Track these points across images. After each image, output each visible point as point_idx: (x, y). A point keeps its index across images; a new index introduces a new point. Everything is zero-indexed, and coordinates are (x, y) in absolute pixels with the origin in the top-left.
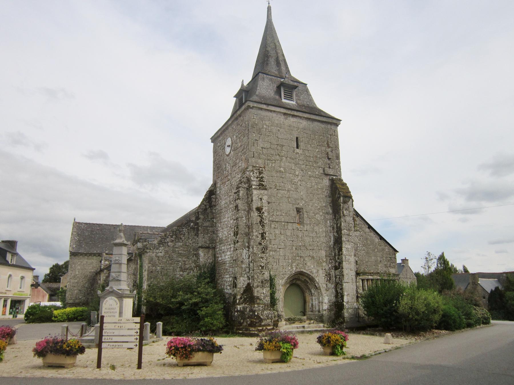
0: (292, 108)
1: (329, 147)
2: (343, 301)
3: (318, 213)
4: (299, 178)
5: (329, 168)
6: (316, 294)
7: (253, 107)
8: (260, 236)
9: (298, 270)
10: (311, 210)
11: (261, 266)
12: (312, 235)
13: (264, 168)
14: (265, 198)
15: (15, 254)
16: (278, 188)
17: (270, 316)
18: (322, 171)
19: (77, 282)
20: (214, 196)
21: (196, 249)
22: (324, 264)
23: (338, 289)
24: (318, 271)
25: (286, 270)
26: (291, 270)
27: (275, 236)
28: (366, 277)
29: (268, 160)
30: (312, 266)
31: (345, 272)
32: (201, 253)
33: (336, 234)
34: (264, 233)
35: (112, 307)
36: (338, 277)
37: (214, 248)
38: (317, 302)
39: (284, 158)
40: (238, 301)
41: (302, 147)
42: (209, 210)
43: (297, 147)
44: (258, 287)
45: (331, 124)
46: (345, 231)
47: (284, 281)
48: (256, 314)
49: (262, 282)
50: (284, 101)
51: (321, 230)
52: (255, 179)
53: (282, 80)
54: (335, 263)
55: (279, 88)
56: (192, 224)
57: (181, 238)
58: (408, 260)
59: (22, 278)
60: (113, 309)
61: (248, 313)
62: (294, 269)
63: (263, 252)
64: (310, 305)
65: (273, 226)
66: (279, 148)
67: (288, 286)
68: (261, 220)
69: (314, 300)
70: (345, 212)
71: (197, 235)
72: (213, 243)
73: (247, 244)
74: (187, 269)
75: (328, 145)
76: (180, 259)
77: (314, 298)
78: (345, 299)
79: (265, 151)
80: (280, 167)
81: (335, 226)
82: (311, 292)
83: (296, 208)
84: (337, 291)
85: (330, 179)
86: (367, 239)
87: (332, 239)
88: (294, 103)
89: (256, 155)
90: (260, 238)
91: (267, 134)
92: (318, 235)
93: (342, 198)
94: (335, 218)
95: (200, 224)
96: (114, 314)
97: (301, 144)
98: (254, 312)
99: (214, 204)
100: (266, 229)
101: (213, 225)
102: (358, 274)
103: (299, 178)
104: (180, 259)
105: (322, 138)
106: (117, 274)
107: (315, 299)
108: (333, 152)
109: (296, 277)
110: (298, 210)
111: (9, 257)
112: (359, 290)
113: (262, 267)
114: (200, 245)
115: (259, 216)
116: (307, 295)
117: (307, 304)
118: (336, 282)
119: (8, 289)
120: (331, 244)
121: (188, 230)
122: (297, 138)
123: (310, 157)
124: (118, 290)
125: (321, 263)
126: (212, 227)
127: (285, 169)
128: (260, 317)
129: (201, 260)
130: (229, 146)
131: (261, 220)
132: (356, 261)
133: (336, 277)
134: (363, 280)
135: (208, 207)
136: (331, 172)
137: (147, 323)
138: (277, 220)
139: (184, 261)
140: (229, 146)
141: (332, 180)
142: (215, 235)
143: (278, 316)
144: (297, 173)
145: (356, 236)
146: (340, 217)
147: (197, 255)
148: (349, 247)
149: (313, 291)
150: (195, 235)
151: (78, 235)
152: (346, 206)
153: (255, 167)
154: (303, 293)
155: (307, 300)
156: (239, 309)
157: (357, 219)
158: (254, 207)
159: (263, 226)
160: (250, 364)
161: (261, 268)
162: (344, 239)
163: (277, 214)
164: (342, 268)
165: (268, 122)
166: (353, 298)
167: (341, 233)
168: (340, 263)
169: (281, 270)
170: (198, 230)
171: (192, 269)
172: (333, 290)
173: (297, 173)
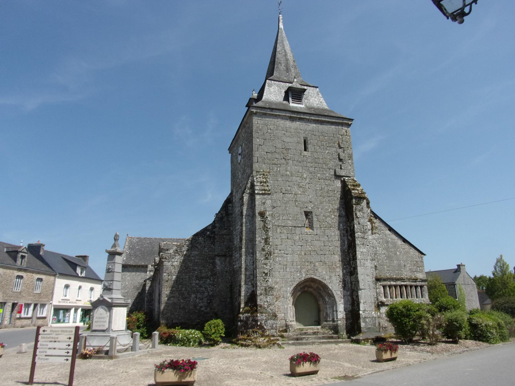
0: (299, 111)
1: (340, 147)
2: (359, 310)
3: (329, 216)
4: (308, 181)
5: (341, 168)
6: (330, 301)
7: (256, 113)
8: (263, 241)
9: (309, 276)
10: (321, 213)
11: (264, 273)
12: (323, 239)
13: (269, 172)
14: (269, 202)
15: (84, 268)
16: (283, 192)
17: (274, 326)
18: (333, 173)
19: (127, 292)
20: (230, 205)
21: (213, 259)
22: (338, 270)
23: (354, 297)
24: (331, 277)
25: (295, 277)
26: (300, 277)
27: (281, 242)
28: (388, 283)
29: (273, 164)
30: (324, 272)
31: (361, 277)
32: (218, 261)
33: (349, 237)
34: (267, 238)
35: (101, 316)
36: (354, 283)
37: (231, 256)
38: (331, 311)
39: (290, 162)
40: (241, 310)
41: (310, 150)
42: (225, 219)
43: (305, 150)
44: (261, 295)
45: (342, 124)
46: (359, 233)
47: (292, 288)
48: (259, 323)
49: (266, 290)
50: (291, 104)
51: (333, 234)
52: (259, 184)
53: (290, 85)
54: (350, 269)
55: (287, 93)
56: (208, 233)
57: (197, 247)
58: (464, 265)
59: (92, 289)
60: (103, 318)
61: (251, 323)
62: (304, 275)
63: (267, 258)
64: (325, 313)
65: (279, 230)
66: (285, 152)
67: (299, 293)
68: (265, 226)
69: (328, 309)
70: (358, 214)
71: (213, 243)
72: (229, 251)
73: (251, 251)
74: (203, 278)
75: (339, 146)
76: (196, 268)
77: (328, 306)
78: (362, 307)
79: (269, 156)
80: (287, 171)
81: (349, 229)
82: (325, 299)
83: (305, 212)
84: (353, 299)
85: (341, 181)
86: (387, 242)
87: (346, 243)
88: (303, 106)
89: (260, 160)
90: (262, 244)
91: (272, 138)
92: (330, 240)
93: (354, 200)
94: (348, 221)
95: (216, 233)
96: (104, 324)
97: (309, 146)
98: (257, 321)
99: (231, 212)
100: (270, 234)
101: (230, 234)
102: (378, 280)
103: (308, 181)
104: (196, 268)
105: (332, 139)
106: (109, 282)
107: (330, 308)
108: (345, 152)
109: (308, 284)
110: (307, 214)
111: (79, 270)
112: (379, 298)
113: (266, 274)
114: (216, 253)
115: (262, 221)
116: (321, 303)
117: (322, 313)
118: (352, 289)
119: (79, 299)
120: (344, 248)
121: (204, 239)
122: (305, 141)
123: (319, 158)
124: (109, 298)
125: (334, 269)
126: (228, 235)
127: (291, 173)
128: (263, 327)
129: (218, 268)
130: (240, 154)
131: (265, 226)
132: (376, 266)
133: (352, 284)
134: (384, 287)
135: (224, 215)
136: (343, 173)
137: (136, 333)
138: (283, 225)
139: (201, 270)
140: (240, 154)
141: (344, 183)
142: (231, 243)
143: (286, 326)
144: (305, 176)
145: (374, 239)
146: (353, 220)
147: (214, 264)
148: (365, 250)
149: (327, 299)
150: (212, 243)
151: (130, 248)
152: (359, 207)
153: (259, 172)
154: (317, 301)
155: (321, 308)
156: (242, 318)
157: (375, 221)
158: (257, 212)
159: (267, 231)
160: (373, 363)
161: (264, 275)
162: (357, 242)
163: (283, 218)
164: (357, 274)
165: (273, 126)
166: (370, 306)
167: (355, 236)
168: (355, 268)
169: (289, 277)
170: (214, 238)
171: (208, 278)
172: (349, 298)
173: (305, 176)
